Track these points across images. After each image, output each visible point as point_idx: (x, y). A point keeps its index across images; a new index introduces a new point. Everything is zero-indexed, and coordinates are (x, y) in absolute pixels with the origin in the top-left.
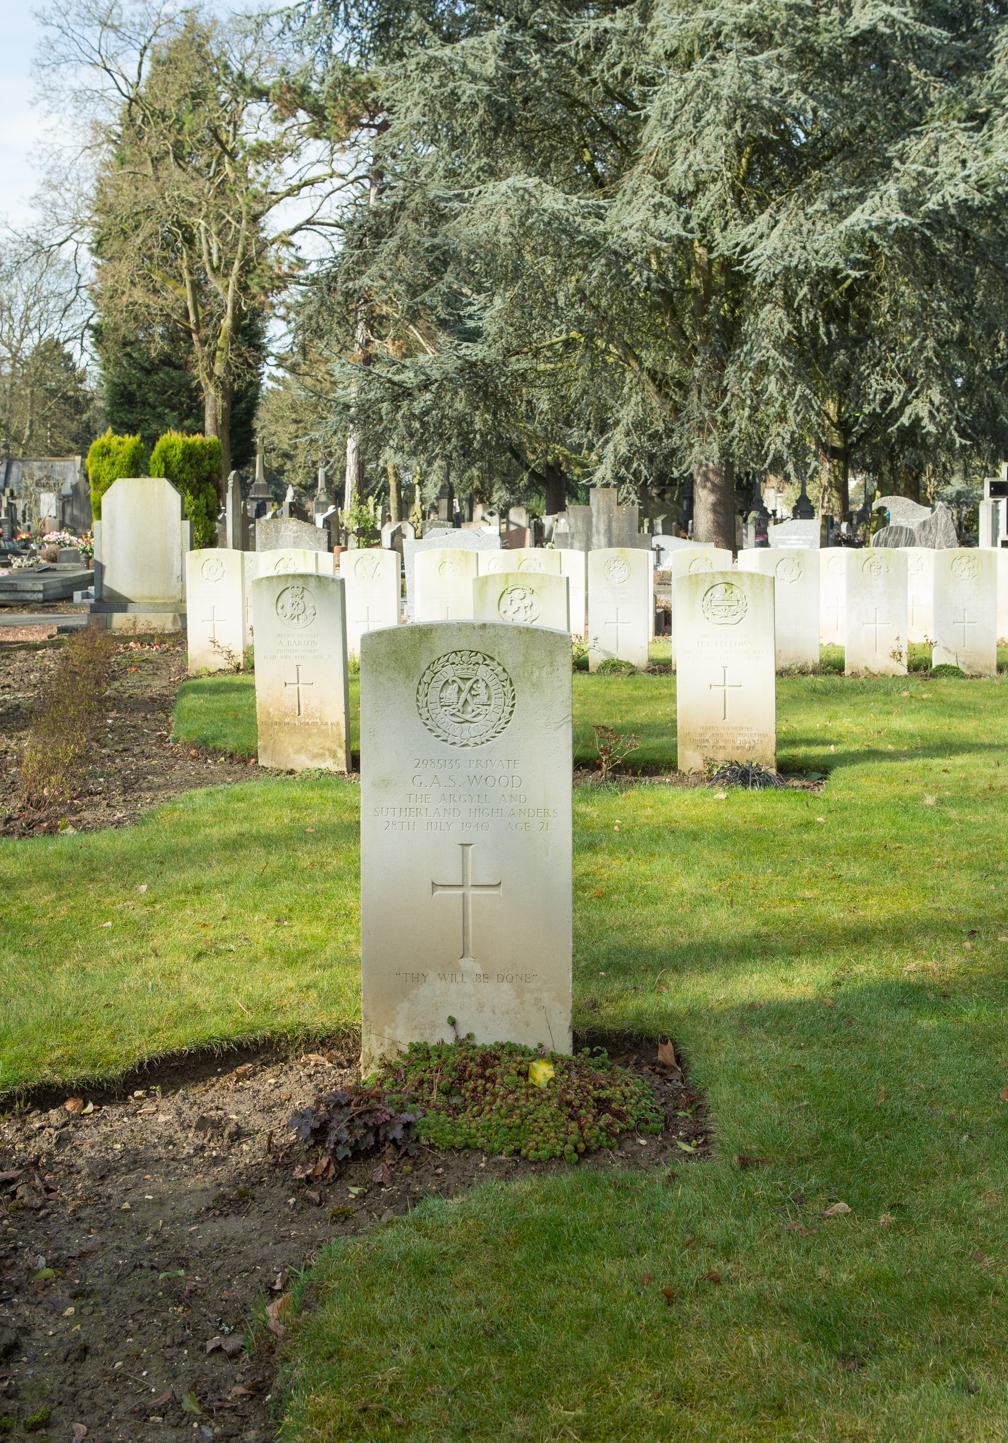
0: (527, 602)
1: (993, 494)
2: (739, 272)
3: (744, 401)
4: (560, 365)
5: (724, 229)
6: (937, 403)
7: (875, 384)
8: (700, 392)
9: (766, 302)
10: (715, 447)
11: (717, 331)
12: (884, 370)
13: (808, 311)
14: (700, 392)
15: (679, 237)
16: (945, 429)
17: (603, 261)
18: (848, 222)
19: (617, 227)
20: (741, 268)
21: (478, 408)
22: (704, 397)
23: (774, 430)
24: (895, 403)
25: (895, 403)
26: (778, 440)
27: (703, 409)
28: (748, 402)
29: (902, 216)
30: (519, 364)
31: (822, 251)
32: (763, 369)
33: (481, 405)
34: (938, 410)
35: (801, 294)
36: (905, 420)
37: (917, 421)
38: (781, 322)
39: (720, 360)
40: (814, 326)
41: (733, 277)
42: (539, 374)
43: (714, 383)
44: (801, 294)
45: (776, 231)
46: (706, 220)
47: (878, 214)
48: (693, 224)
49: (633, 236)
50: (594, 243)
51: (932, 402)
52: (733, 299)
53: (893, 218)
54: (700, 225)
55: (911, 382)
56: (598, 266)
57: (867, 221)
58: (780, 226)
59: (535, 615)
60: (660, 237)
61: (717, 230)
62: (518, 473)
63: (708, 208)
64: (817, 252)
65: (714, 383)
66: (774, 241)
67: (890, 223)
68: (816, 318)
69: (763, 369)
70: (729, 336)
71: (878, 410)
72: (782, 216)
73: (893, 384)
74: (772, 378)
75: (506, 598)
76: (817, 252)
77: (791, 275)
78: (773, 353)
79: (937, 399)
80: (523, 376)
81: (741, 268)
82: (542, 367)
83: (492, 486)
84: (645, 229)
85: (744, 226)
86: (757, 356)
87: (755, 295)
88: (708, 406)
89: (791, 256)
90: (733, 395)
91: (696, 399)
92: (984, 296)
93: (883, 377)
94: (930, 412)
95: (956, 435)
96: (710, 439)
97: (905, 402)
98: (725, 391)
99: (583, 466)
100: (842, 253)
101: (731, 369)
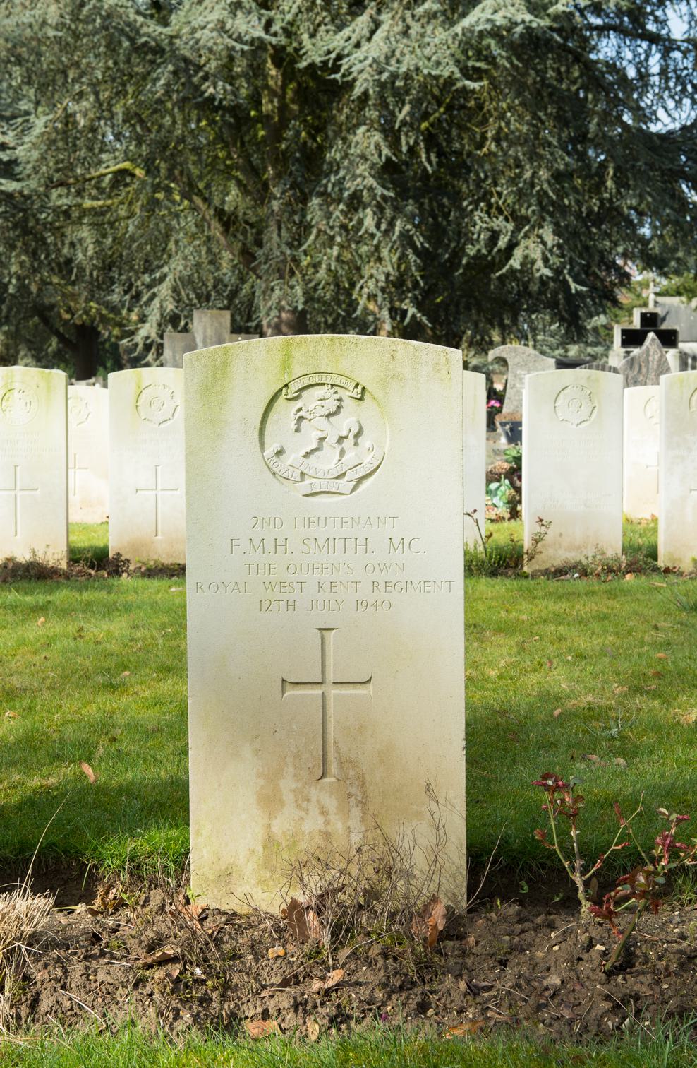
0: (345, 423)
1: (625, 343)
2: (335, 80)
3: (332, 238)
4: (109, 202)
5: (312, 36)
6: (550, 244)
7: (480, 222)
8: (279, 229)
9: (358, 126)
10: (299, 290)
11: (297, 160)
12: (490, 206)
13: (407, 135)
14: (279, 229)
15: (260, 39)
16: (558, 272)
17: (170, 67)
18: (466, 22)
19: (186, 30)
20: (338, 76)
21: (13, 247)
22: (284, 233)
23: (366, 271)
24: (502, 242)
25: (502, 242)
26: (371, 284)
27: (284, 247)
28: (338, 239)
29: (528, 17)
30: (59, 199)
31: (434, 58)
32: (355, 203)
33: (19, 244)
34: (551, 251)
35: (400, 117)
36: (515, 263)
37: (527, 262)
38: (378, 147)
39: (302, 192)
40: (412, 151)
41: (321, 90)
42: (84, 213)
43: (296, 218)
44: (400, 117)
45: (380, 34)
46: (291, 24)
47: (501, 13)
48: (276, 27)
49: (205, 36)
50: (154, 52)
51: (544, 243)
52: (312, 126)
53: (519, 18)
54: (284, 29)
55: (520, 221)
56: (164, 74)
57: (488, 20)
58: (385, 27)
59: (369, 462)
60: (239, 39)
61: (305, 37)
62: (46, 340)
63: (294, 10)
64: (429, 59)
65: (296, 218)
66: (376, 48)
67: (516, 24)
68: (416, 143)
69: (355, 203)
70: (309, 168)
71: (484, 251)
72: (385, 17)
73: (499, 223)
74: (368, 211)
75: (285, 412)
76: (429, 59)
77: (391, 89)
78: (371, 181)
79: (550, 239)
80: (67, 214)
81: (338, 76)
82: (88, 203)
83: (17, 352)
84: (221, 28)
85: (335, 33)
86: (351, 186)
87: (343, 118)
88: (290, 245)
89: (398, 61)
90: (319, 231)
91: (275, 236)
92: (598, 125)
93: (488, 213)
94: (543, 254)
95: (570, 280)
96: (293, 282)
97: (512, 246)
98: (308, 227)
99: (120, 325)
100: (458, 62)
101: (315, 201)
